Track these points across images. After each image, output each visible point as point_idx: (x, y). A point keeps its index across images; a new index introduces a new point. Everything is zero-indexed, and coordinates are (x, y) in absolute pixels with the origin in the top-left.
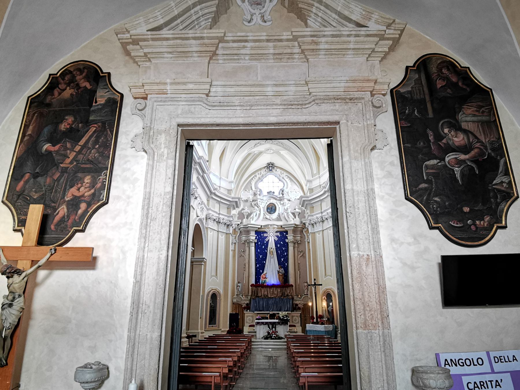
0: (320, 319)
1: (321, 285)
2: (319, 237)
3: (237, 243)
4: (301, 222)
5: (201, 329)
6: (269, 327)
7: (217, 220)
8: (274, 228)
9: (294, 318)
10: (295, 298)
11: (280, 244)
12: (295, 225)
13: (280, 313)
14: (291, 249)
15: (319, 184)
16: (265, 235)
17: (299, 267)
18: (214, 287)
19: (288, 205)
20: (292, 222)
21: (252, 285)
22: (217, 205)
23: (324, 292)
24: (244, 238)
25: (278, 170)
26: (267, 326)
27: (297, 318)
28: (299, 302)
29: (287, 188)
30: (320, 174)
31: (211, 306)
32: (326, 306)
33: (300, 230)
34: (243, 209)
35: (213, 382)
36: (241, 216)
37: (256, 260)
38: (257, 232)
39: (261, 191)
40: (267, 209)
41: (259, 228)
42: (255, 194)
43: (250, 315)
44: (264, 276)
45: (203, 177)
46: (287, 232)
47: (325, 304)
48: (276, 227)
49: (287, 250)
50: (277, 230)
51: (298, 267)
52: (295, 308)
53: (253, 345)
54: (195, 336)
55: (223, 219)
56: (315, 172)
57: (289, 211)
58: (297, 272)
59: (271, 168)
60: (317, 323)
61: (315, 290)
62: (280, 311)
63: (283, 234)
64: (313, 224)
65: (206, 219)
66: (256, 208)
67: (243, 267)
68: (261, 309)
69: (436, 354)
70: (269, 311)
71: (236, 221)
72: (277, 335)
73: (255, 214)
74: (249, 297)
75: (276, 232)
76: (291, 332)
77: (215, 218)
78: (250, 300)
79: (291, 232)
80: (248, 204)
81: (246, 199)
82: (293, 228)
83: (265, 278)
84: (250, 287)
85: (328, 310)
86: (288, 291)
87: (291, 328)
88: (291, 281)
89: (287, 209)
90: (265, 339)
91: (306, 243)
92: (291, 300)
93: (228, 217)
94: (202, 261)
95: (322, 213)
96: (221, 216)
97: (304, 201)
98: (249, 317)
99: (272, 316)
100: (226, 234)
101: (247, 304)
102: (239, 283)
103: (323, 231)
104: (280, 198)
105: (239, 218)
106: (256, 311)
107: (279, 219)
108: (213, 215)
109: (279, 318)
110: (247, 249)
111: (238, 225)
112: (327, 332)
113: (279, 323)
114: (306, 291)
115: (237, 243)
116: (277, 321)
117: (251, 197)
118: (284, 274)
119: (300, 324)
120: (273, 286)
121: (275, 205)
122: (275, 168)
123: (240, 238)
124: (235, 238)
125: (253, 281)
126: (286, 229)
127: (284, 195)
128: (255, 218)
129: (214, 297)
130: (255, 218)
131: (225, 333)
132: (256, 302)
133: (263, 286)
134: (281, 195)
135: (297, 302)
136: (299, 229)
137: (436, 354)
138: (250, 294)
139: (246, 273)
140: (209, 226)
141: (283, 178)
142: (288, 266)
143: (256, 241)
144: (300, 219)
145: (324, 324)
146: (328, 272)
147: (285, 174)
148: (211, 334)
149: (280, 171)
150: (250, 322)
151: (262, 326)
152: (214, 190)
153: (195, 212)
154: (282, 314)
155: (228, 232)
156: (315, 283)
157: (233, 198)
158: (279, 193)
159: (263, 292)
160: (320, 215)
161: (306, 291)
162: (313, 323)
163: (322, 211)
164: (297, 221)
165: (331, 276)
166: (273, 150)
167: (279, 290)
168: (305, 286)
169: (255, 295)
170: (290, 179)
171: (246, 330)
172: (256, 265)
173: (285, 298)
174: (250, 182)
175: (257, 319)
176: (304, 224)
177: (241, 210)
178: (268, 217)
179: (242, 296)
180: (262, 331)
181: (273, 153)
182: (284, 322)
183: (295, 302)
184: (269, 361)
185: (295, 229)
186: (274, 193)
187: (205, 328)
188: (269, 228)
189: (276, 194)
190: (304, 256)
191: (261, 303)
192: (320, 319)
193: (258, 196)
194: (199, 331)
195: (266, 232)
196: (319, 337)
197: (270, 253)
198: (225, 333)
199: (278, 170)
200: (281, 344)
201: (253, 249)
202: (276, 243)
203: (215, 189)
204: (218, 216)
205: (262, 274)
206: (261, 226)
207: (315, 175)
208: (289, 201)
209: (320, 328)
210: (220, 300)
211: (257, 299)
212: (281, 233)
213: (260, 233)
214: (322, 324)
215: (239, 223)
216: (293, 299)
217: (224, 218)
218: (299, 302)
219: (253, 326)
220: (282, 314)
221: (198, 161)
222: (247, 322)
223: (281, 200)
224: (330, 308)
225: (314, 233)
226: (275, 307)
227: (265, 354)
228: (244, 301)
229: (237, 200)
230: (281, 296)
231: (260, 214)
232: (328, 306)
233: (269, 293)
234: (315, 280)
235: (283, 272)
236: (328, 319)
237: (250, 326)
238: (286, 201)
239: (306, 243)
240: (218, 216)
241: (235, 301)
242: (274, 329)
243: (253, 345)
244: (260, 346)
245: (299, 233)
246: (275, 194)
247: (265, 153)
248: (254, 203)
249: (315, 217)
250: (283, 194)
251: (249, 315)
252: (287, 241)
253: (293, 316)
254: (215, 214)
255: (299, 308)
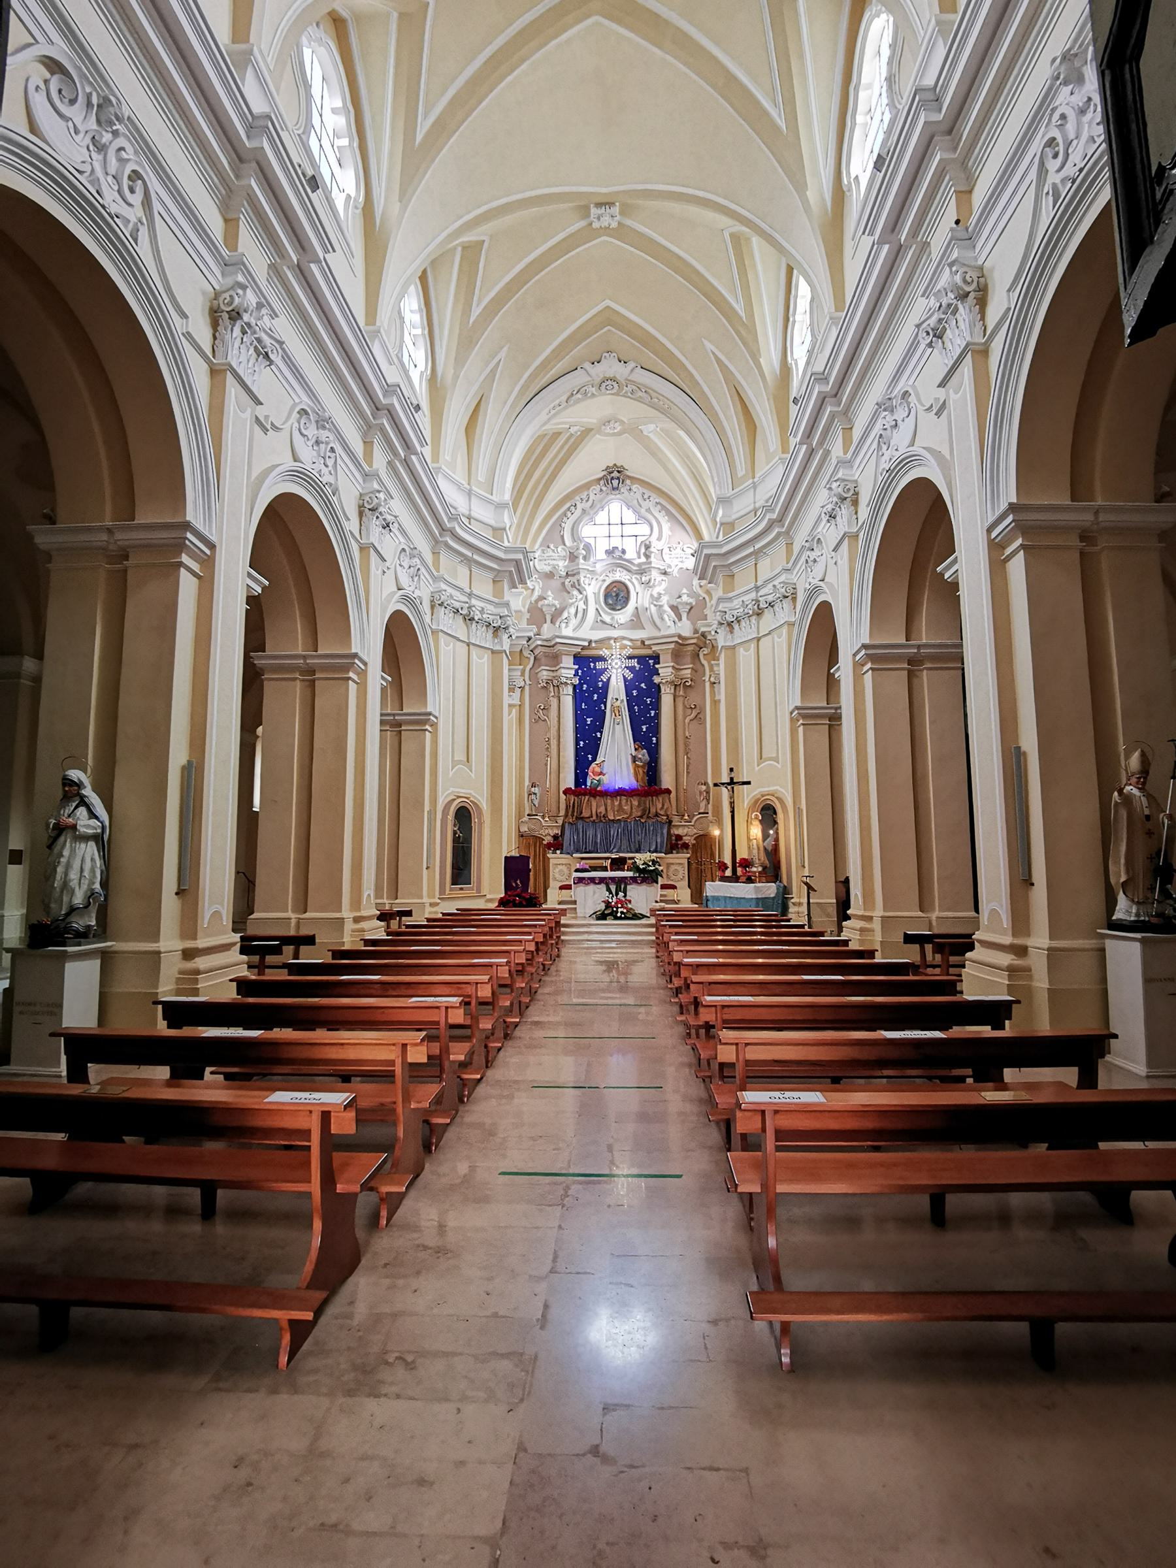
0: (741, 870)
1: (748, 783)
2: (745, 657)
3: (527, 688)
4: (696, 631)
5: (431, 896)
6: (609, 890)
7: (464, 612)
8: (623, 647)
9: (673, 868)
10: (676, 821)
11: (639, 689)
12: (680, 636)
13: (637, 855)
14: (666, 700)
15: (752, 507)
16: (600, 665)
17: (686, 745)
18: (462, 792)
19: (661, 586)
20: (672, 631)
21: (567, 791)
22: (463, 571)
23: (756, 801)
24: (544, 674)
25: (634, 487)
26: (603, 887)
27: (679, 868)
28: (686, 830)
29: (659, 539)
30: (757, 475)
31: (456, 840)
32: (760, 835)
33: (695, 650)
34: (542, 598)
35: (399, 1062)
36: (537, 615)
37: (577, 730)
38: (579, 659)
39: (587, 547)
40: (606, 596)
41: (584, 648)
42: (573, 557)
43: (563, 861)
44: (598, 770)
45: (407, 463)
46: (656, 658)
47: (756, 831)
48: (629, 643)
49: (657, 705)
50: (630, 652)
51: (683, 745)
52: (675, 845)
53: (565, 933)
54: (409, 913)
55: (482, 611)
56: (740, 473)
57: (664, 600)
58: (680, 760)
59: (615, 482)
60: (735, 878)
61: (732, 797)
62: (638, 851)
63: (645, 664)
64: (730, 624)
65: (432, 607)
66: (575, 592)
67: (541, 748)
68: (590, 848)
69: (905, 942)
70: (611, 852)
71: (521, 628)
72: (629, 910)
73: (573, 610)
74: (560, 821)
75: (630, 658)
76: (666, 902)
77: (457, 605)
78: (563, 826)
79: (669, 656)
80: (556, 583)
81: (548, 569)
82: (672, 646)
83: (601, 773)
84: (563, 797)
85: (765, 849)
86: (658, 804)
87: (665, 892)
88: (667, 780)
89: (660, 594)
90: (598, 918)
91: (708, 684)
92: (666, 826)
93: (497, 605)
94: (425, 722)
95: (757, 588)
96: (474, 602)
97: (708, 557)
98: (561, 866)
99: (618, 864)
100: (493, 652)
101: (555, 837)
102: (533, 785)
103: (759, 639)
104: (639, 565)
105: (529, 622)
106: (577, 851)
107: (637, 622)
108: (451, 596)
109: (635, 868)
110: (554, 702)
111: (530, 639)
112: (763, 902)
113: (634, 880)
114: (703, 805)
115: (527, 688)
116: (630, 874)
117: (562, 565)
118: (649, 764)
119: (686, 883)
120: (621, 792)
121: (628, 592)
122: (628, 482)
123: (534, 675)
124: (523, 674)
125: (569, 781)
126: (654, 648)
127: (652, 559)
128: (574, 622)
129: (463, 816)
130: (574, 622)
131: (493, 905)
132: (577, 829)
133: (594, 793)
134: (643, 559)
135: (680, 832)
136: (690, 648)
137: (905, 942)
138: (562, 813)
139: (552, 763)
140: (441, 627)
141: (648, 510)
142: (658, 744)
143: (576, 681)
144: (694, 624)
145: (752, 881)
146: (768, 751)
147: (655, 498)
148: (451, 907)
149: (642, 490)
150: (563, 878)
151: (592, 887)
152: (450, 519)
153: (390, 574)
154: (641, 858)
155: (497, 648)
156: (732, 779)
157: (507, 550)
158: (638, 553)
159: (595, 807)
160: (753, 595)
161: (703, 805)
162: (724, 879)
163: (759, 583)
164: (685, 628)
165: (776, 760)
166: (622, 422)
167: (635, 803)
168: (701, 793)
169: (575, 816)
170: (669, 513)
171: (553, 898)
172: (577, 744)
173: (650, 821)
174: (559, 524)
175: (577, 871)
176: (703, 635)
177: (537, 601)
178: (607, 619)
179: (543, 817)
180: (592, 898)
181: (620, 434)
182: (648, 876)
183: (675, 831)
184: (609, 970)
185: (680, 649)
186: (624, 552)
187: (442, 891)
188: (609, 648)
189: (631, 554)
190: (699, 718)
191: (590, 833)
192: (741, 870)
193: (582, 561)
194: (426, 900)
195: (602, 659)
196: (741, 916)
197: (613, 711)
198: (493, 905)
199: (634, 487)
200: (643, 931)
201: (568, 702)
202: (629, 686)
203: (454, 518)
204: (466, 599)
205: (593, 765)
206: (590, 642)
207: (744, 479)
208: (665, 573)
209: (744, 891)
210: (481, 824)
211: (580, 824)
212: (641, 659)
213: (587, 662)
214: (749, 880)
215: (531, 634)
216: (670, 822)
217: (484, 609)
218: (686, 831)
219: (568, 887)
220: (641, 858)
221: (384, 401)
222: (555, 879)
223: (642, 571)
224: (770, 842)
225: (734, 647)
226: (625, 842)
227: (599, 957)
228: (548, 830)
229: (520, 556)
230: (641, 817)
231: (585, 611)
232: (765, 836)
233: (612, 809)
234: (731, 770)
235: (647, 757)
236: (765, 868)
237: (561, 888)
238: (655, 574)
239: (708, 684)
240: (466, 599)
241: (524, 829)
242: (621, 894)
243: (565, 933)
244: (585, 937)
245: (688, 659)
246: (627, 556)
247: (599, 432)
248: (570, 582)
249: (737, 603)
250: (647, 556)
251: (560, 861)
252: (656, 680)
253: (669, 865)
254: (456, 594)
255: (686, 846)
